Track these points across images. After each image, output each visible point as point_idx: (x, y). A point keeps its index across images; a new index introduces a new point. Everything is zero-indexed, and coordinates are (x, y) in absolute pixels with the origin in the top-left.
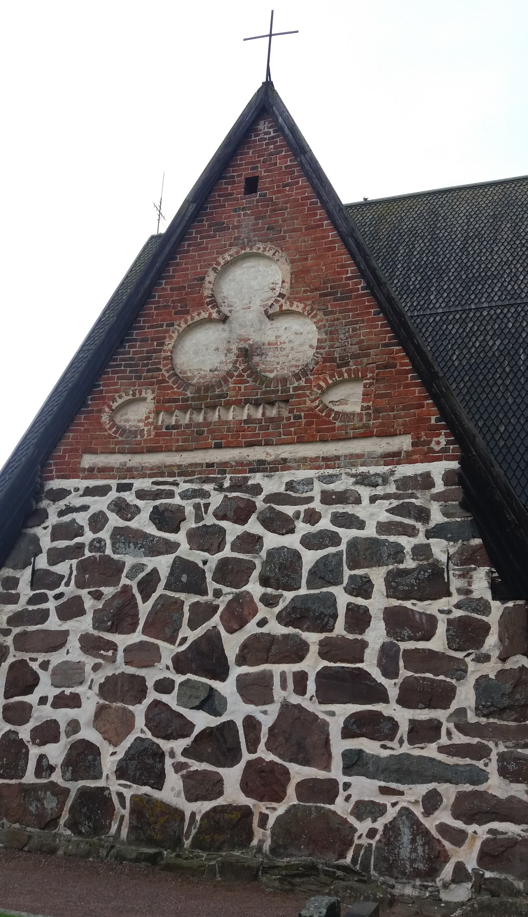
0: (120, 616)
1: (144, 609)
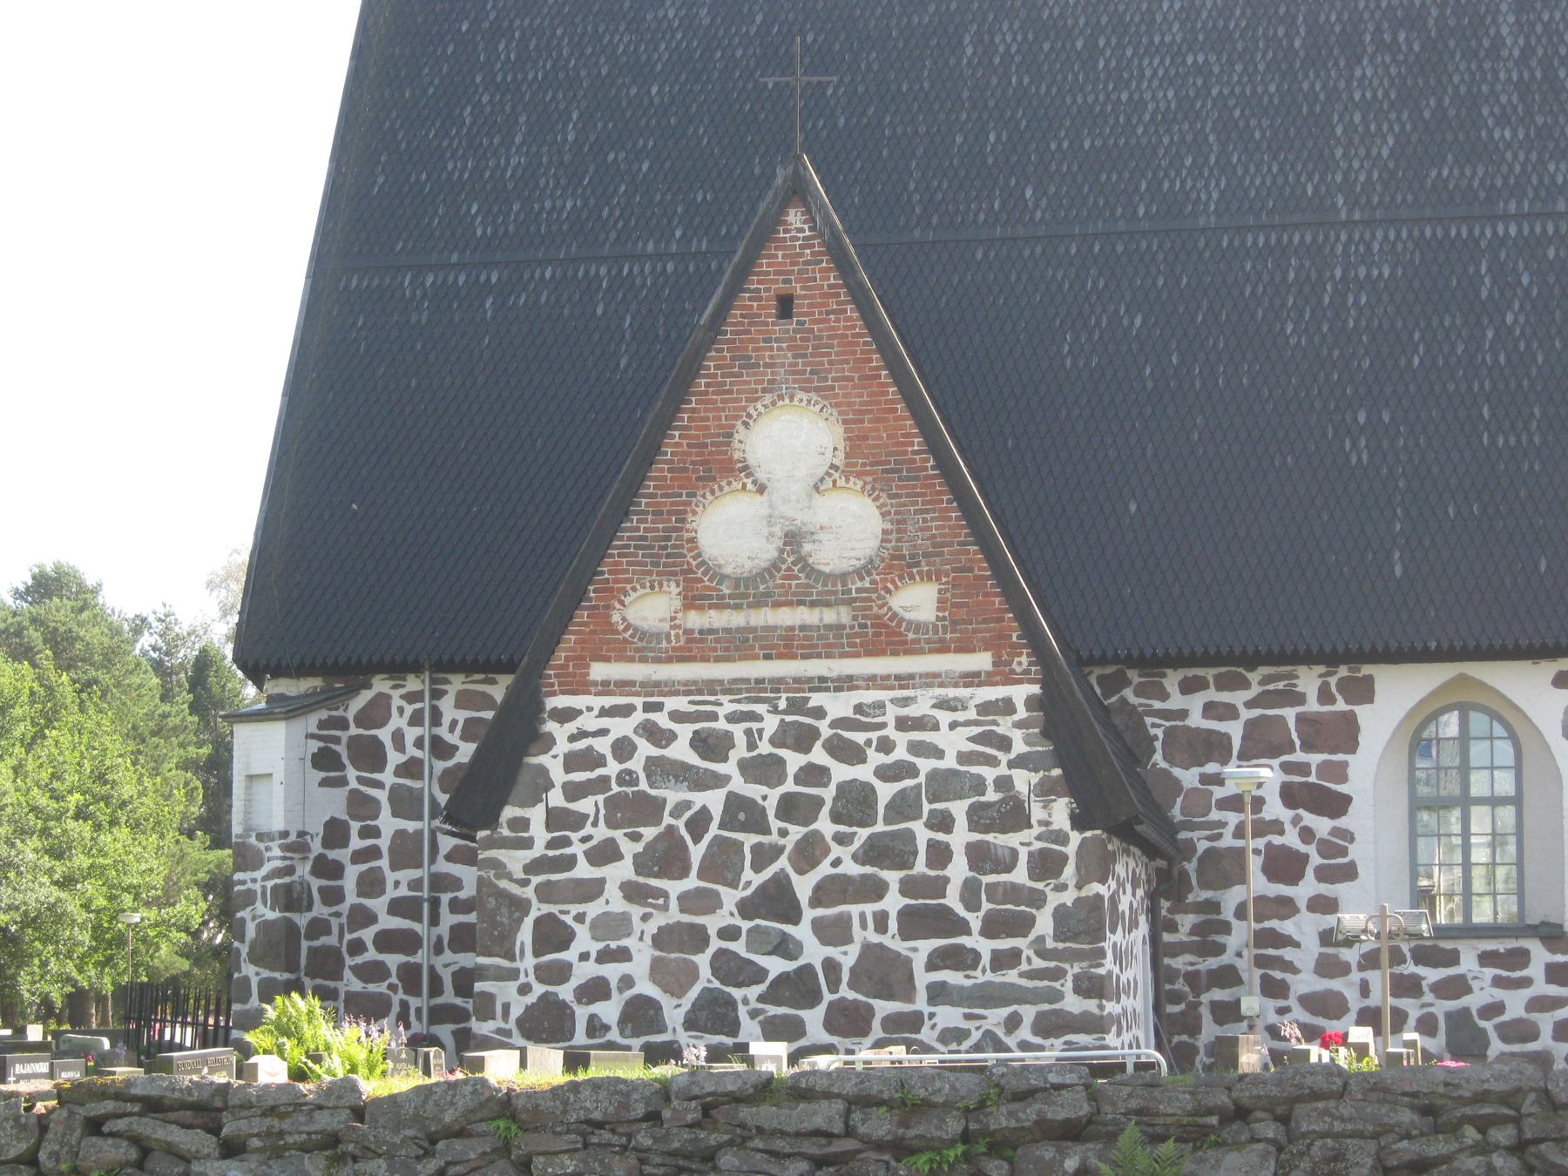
1: (697, 852)
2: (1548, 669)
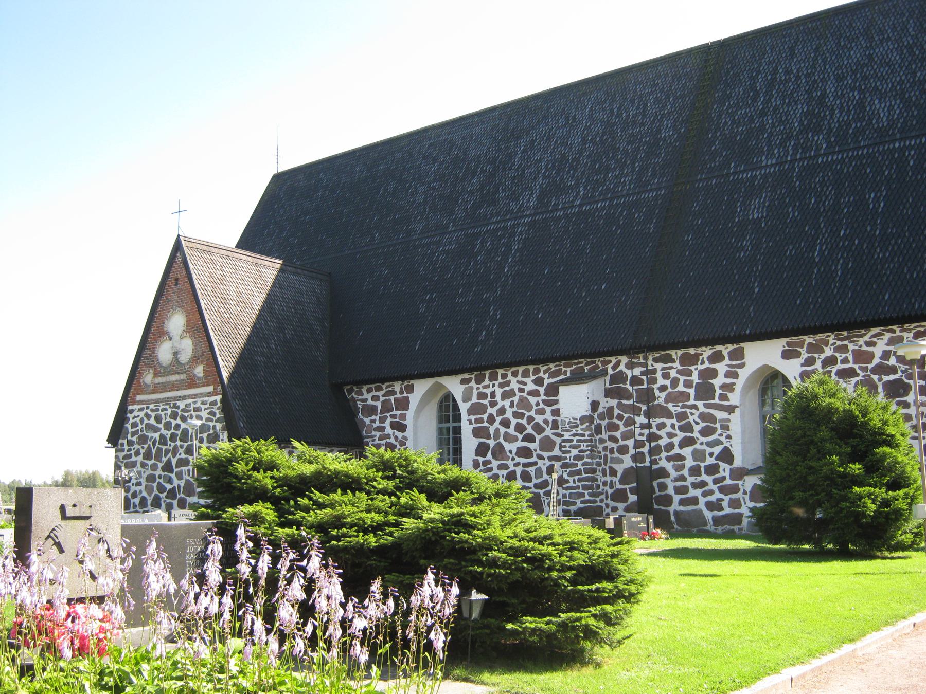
0: (148, 456)
2: (459, 378)
